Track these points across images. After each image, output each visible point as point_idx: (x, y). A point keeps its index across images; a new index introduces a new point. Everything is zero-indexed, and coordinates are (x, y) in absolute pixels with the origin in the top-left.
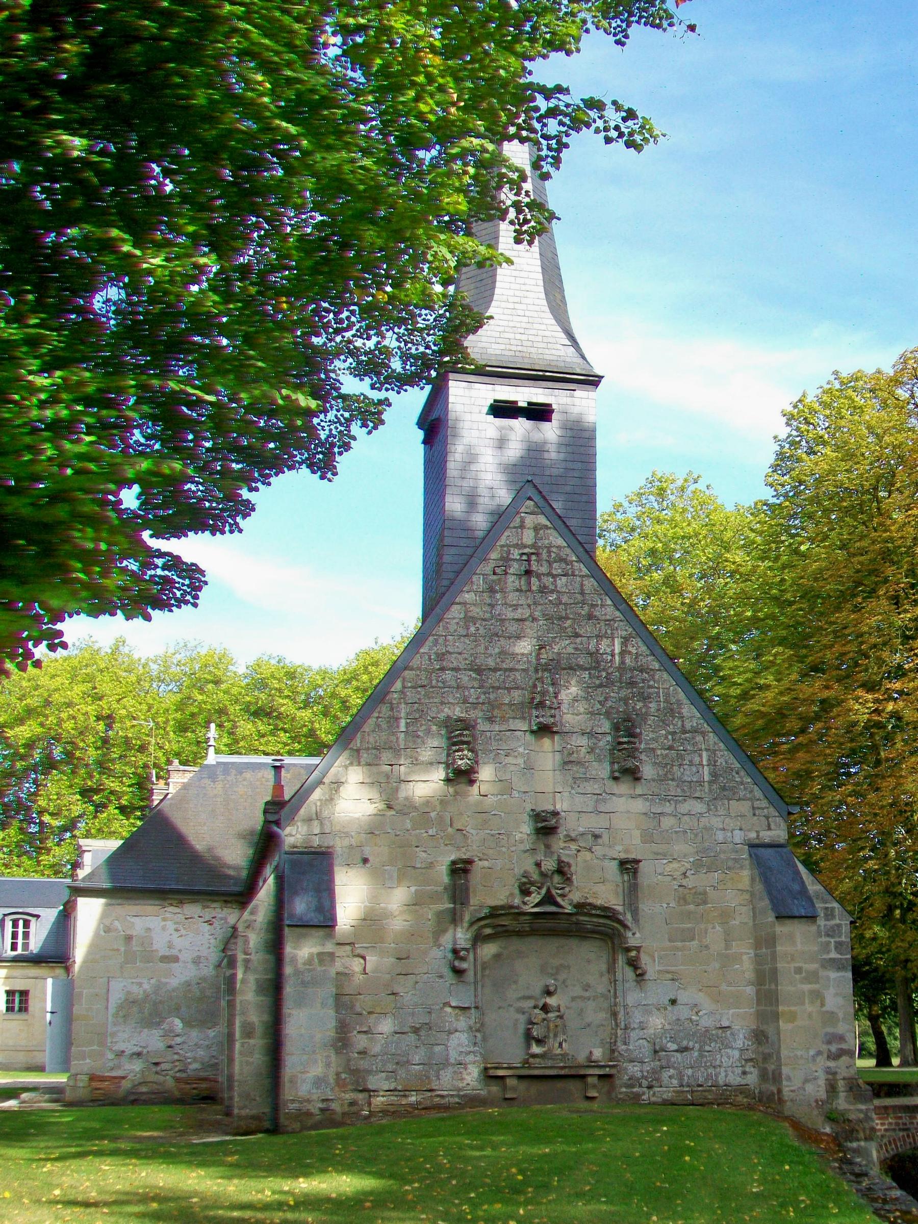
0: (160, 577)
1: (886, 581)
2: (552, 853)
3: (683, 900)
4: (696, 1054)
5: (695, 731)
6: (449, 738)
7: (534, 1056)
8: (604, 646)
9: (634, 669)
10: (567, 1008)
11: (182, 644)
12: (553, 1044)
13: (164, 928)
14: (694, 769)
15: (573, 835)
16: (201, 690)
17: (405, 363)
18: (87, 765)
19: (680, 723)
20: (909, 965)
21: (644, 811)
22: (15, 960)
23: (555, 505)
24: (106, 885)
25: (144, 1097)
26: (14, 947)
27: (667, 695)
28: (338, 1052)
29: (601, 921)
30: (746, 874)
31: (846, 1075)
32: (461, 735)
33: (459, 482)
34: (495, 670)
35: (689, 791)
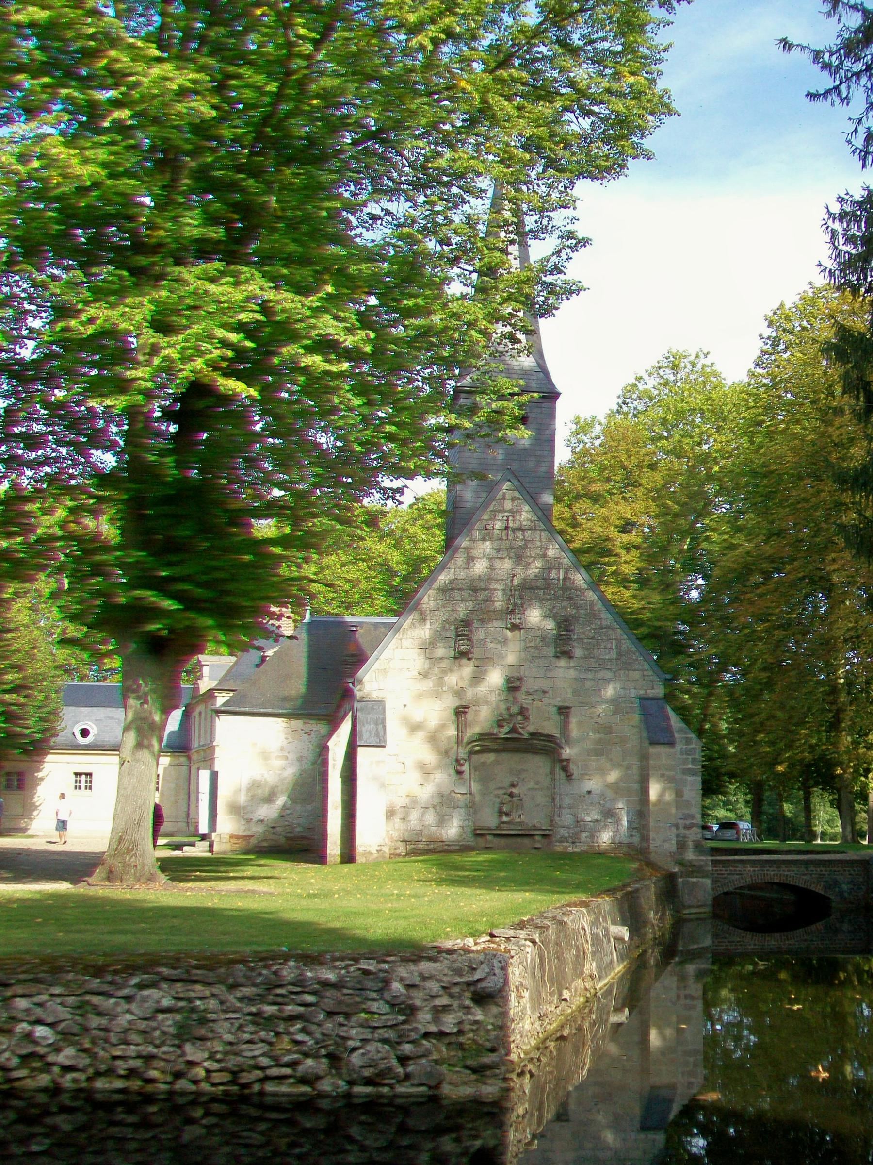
5: (608, 627)
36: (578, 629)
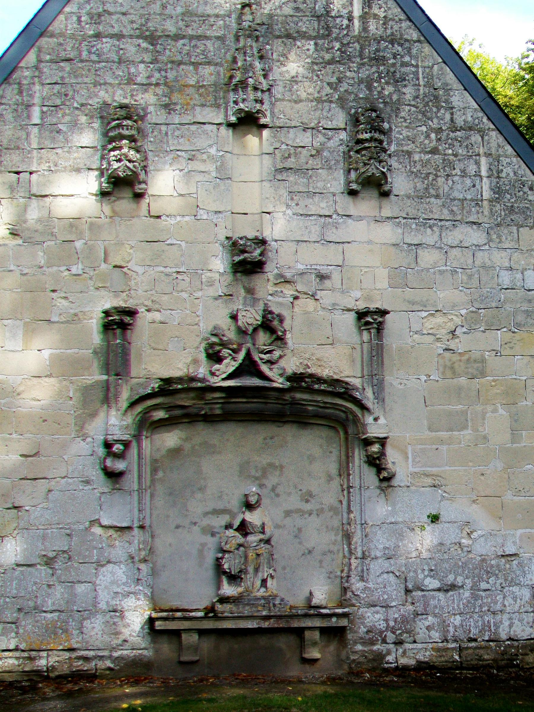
2: (255, 301)
3: (451, 370)
4: (467, 594)
6: (105, 134)
7: (223, 600)
10: (277, 526)
12: (252, 582)
19: (448, 117)
21: (393, 241)
27: (429, 77)
29: (329, 400)
32: (119, 126)
34: (177, 37)
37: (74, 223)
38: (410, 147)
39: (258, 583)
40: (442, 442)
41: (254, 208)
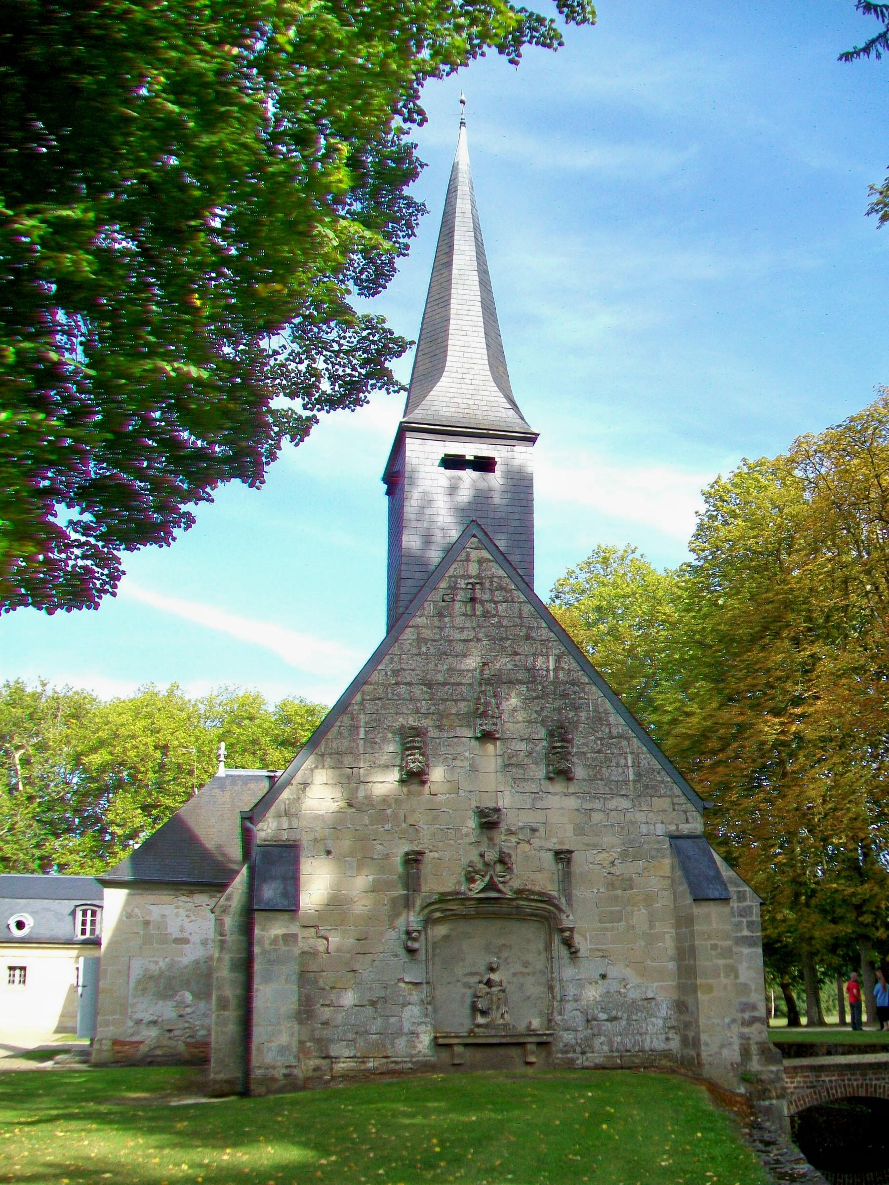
0: (81, 567)
1: (788, 626)
3: (611, 886)
4: (624, 1023)
5: (620, 736)
6: (403, 744)
8: (540, 662)
9: (567, 683)
10: (509, 983)
11: (223, 688)
12: (495, 1014)
13: (177, 915)
14: (620, 770)
15: (513, 829)
16: (239, 725)
17: (333, 384)
18: (147, 786)
19: (607, 730)
20: (813, 942)
22: (85, 942)
23: (498, 543)
24: (128, 877)
25: (159, 1059)
26: (83, 932)
27: (596, 706)
28: (301, 1022)
30: (667, 862)
31: (758, 1040)
33: (414, 524)
34: (444, 684)
35: (616, 789)
36: (578, 740)
37: (385, 800)
38: (585, 749)
39: (499, 1016)
40: (607, 929)
41: (492, 787)
